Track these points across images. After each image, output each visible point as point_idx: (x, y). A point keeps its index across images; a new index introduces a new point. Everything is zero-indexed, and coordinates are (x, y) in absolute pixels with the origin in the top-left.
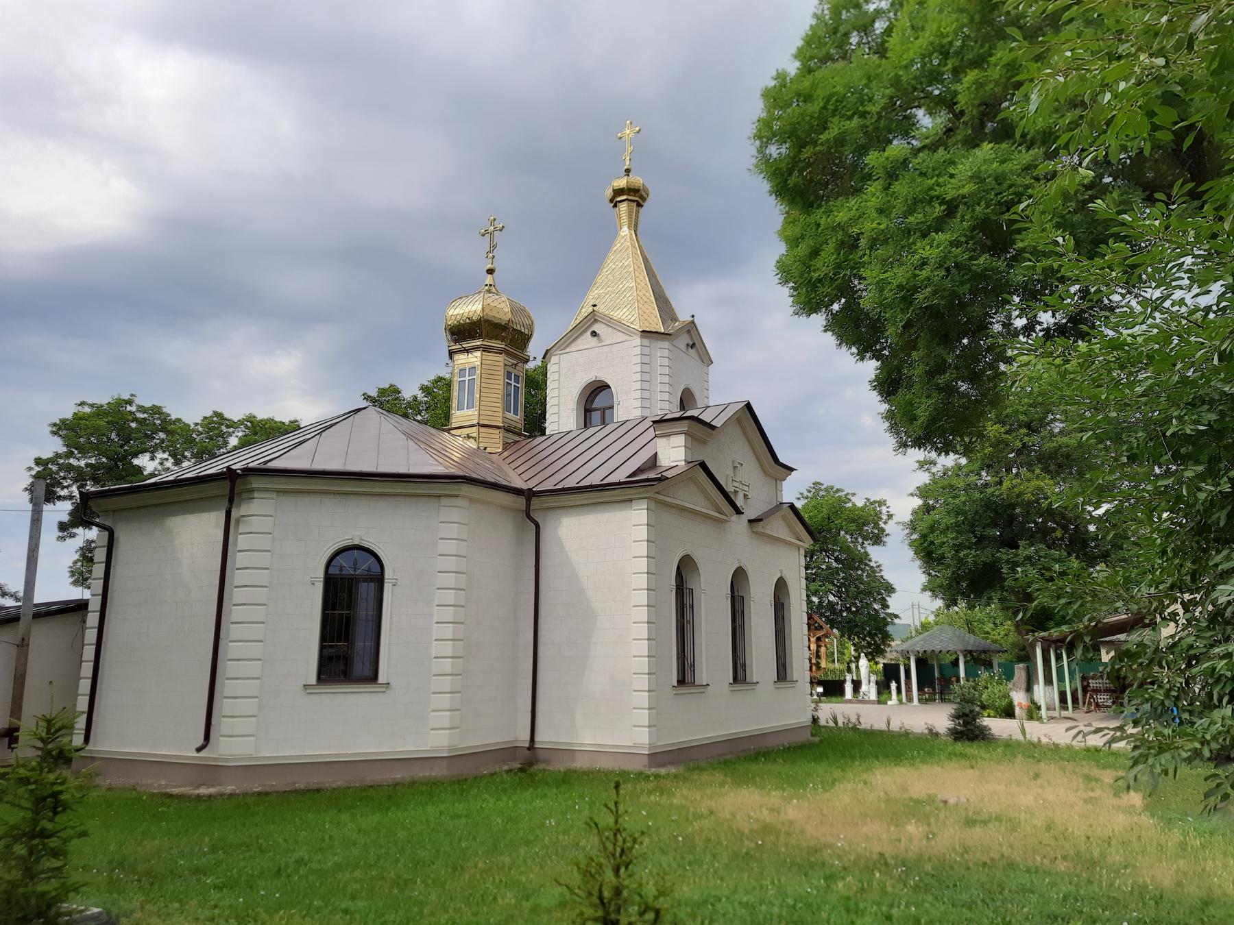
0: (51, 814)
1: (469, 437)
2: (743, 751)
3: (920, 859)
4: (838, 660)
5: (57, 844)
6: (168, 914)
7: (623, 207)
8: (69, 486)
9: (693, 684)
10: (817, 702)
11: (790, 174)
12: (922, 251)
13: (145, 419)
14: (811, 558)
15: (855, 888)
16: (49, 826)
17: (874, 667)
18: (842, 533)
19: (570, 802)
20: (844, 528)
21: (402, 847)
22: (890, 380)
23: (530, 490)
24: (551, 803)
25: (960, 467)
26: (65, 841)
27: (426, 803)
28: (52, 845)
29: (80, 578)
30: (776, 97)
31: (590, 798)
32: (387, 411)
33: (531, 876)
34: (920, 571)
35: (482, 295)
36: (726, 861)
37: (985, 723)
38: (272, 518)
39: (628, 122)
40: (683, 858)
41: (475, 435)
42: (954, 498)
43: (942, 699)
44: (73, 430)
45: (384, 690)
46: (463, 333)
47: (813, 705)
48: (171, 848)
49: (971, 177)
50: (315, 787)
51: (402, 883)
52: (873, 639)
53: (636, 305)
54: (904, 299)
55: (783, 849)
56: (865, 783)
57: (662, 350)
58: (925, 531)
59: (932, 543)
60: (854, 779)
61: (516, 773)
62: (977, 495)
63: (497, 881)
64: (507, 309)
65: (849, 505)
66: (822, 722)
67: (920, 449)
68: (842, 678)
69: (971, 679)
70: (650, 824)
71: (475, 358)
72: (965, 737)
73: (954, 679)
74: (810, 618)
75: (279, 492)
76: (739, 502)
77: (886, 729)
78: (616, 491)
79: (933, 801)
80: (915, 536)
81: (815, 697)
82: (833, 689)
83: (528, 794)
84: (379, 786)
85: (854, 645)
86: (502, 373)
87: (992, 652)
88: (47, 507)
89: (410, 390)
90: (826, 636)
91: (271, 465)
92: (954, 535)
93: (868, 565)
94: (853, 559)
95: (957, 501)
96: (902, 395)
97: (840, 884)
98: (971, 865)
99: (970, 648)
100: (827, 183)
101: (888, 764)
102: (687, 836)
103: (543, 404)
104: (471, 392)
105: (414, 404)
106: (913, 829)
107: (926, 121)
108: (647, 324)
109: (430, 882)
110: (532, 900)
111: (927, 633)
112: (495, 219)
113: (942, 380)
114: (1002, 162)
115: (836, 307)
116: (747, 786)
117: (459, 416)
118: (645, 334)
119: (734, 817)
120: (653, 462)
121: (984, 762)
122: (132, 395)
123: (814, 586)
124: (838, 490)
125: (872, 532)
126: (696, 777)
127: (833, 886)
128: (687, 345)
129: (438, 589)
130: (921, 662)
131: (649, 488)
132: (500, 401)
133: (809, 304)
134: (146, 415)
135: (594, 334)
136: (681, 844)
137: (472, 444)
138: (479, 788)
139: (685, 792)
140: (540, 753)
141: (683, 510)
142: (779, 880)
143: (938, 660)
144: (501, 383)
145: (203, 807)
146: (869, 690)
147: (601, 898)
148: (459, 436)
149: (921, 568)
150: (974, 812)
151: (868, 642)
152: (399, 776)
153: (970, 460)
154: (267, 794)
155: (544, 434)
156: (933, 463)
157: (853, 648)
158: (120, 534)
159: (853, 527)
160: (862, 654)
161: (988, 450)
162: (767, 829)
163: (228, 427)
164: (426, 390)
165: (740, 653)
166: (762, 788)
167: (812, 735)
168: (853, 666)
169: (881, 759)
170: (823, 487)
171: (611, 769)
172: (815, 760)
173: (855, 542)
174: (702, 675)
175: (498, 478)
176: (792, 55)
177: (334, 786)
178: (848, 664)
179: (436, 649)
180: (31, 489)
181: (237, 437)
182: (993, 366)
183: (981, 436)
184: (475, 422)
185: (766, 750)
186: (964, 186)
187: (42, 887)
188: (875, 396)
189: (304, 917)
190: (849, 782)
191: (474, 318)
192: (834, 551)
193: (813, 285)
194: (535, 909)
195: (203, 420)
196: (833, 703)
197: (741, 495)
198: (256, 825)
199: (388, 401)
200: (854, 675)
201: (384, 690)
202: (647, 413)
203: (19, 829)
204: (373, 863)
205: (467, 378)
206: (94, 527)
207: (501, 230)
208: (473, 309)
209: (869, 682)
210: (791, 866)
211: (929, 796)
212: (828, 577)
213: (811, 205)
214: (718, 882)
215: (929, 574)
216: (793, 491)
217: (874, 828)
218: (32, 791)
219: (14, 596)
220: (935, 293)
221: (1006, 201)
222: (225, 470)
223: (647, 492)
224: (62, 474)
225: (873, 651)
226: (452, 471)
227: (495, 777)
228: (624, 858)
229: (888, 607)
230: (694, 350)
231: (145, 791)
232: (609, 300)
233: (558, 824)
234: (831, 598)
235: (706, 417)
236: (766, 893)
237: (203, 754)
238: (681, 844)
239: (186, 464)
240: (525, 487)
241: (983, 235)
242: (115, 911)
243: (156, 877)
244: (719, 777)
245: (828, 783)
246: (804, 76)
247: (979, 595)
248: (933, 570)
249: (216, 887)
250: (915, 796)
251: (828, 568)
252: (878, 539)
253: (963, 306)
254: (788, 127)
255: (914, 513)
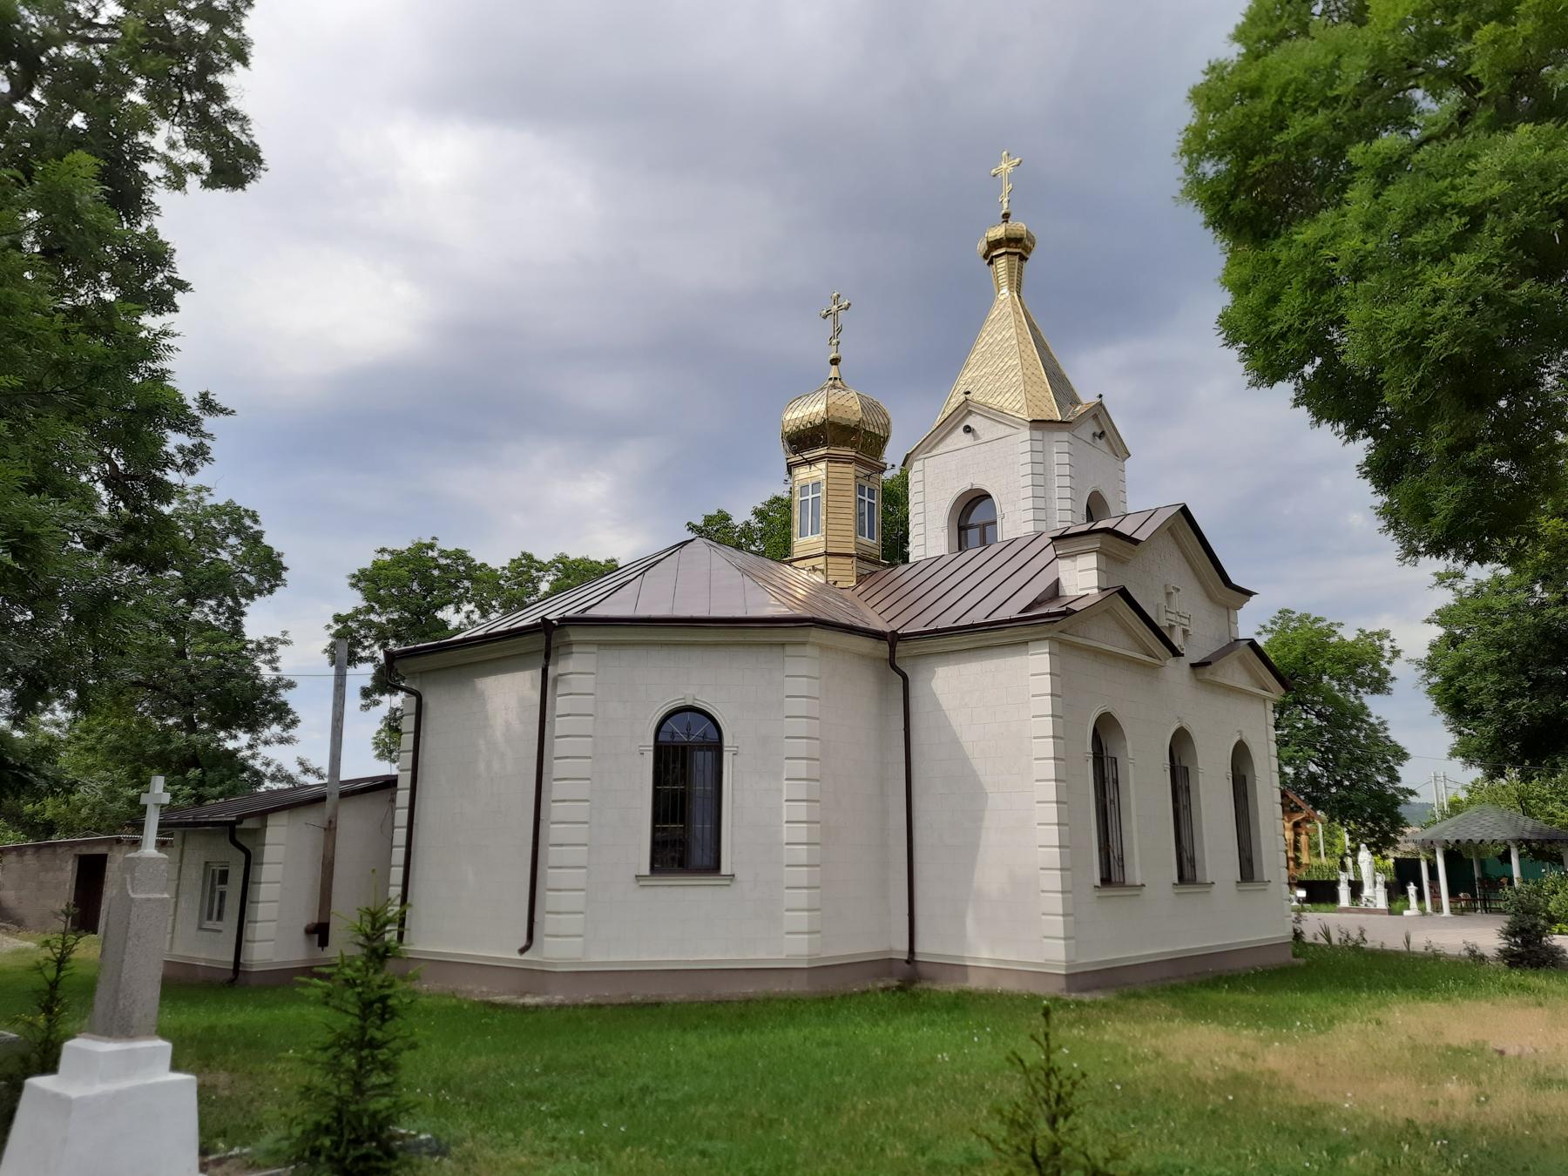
0: (378, 1022)
1: (814, 569)
2: (1196, 974)
3: (1468, 1129)
4: (1325, 854)
5: (385, 1057)
6: (502, 1146)
7: (1002, 263)
8: (371, 646)
9: (1122, 884)
10: (1299, 911)
11: (1233, 196)
12: (1437, 280)
13: (448, 565)
14: (1281, 714)
15: (1373, 1164)
16: (379, 1035)
17: (1380, 863)
18: (1325, 678)
19: (967, 1032)
20: (1328, 671)
21: (763, 1079)
22: (1387, 463)
23: (894, 632)
24: (942, 1033)
25: (1500, 581)
26: (397, 1052)
27: (787, 1026)
28: (381, 1057)
29: (386, 750)
30: (1208, 97)
31: (993, 1029)
32: (718, 543)
33: (926, 1124)
34: (1446, 729)
35: (825, 392)
36: (1186, 1120)
37: (1555, 943)
38: (593, 676)
39: (1005, 153)
40: (1124, 1112)
41: (822, 567)
42: (1494, 624)
43: (1486, 909)
44: (375, 582)
45: (728, 882)
46: (803, 441)
47: (1294, 915)
48: (499, 1067)
49: (1502, 174)
50: (654, 1000)
51: (766, 1123)
52: (1377, 824)
53: (1022, 388)
54: (1408, 350)
55: (1265, 1109)
56: (1379, 1023)
57: (1059, 448)
58: (1451, 673)
59: (1462, 689)
60: (1361, 1018)
61: (894, 992)
62: (1529, 619)
63: (883, 1127)
64: (857, 407)
65: (1334, 640)
66: (1308, 938)
67: (1438, 557)
68: (1333, 878)
69: (1531, 881)
70: (1075, 1065)
71: (819, 471)
72: (1525, 962)
73: (1504, 880)
74: (1284, 795)
75: (600, 644)
76: (1177, 640)
77: (1405, 949)
78: (1006, 631)
79: (1482, 1049)
80: (1435, 680)
81: (1295, 903)
82: (1321, 892)
83: (912, 1019)
84: (728, 1002)
85: (1349, 832)
86: (853, 487)
87: (1562, 841)
88: (350, 671)
89: (741, 515)
90: (1307, 820)
91: (591, 613)
92: (1496, 677)
93: (1366, 722)
94: (1342, 714)
95: (1498, 629)
96: (1409, 483)
97: (1352, 1160)
98: (1548, 1142)
99: (1527, 836)
100: (1287, 205)
101: (1410, 997)
102: (1127, 1084)
103: (905, 523)
104: (815, 514)
105: (747, 530)
106: (1455, 1089)
107: (1428, 105)
108: (1037, 411)
109: (801, 1123)
110: (929, 1155)
111: (1459, 816)
112: (839, 296)
113: (1473, 457)
114: (1548, 149)
115: (1308, 370)
116: (1206, 1021)
117: (804, 543)
118: (1034, 424)
119: (1191, 1062)
120: (1054, 591)
121: (1557, 998)
122: (434, 538)
123: (1289, 751)
124: (1317, 620)
125: (1370, 676)
126: (1132, 1007)
127: (1341, 1161)
128: (1094, 434)
129: (787, 758)
130: (1453, 856)
131: (1049, 626)
132: (853, 523)
133: (1268, 370)
134: (449, 561)
135: (968, 429)
136: (1120, 1095)
137: (819, 578)
138: (849, 1008)
139: (1119, 1026)
140: (921, 968)
141: (1097, 653)
142: (1263, 1149)
143: (1479, 853)
144: (852, 500)
145: (530, 1019)
146: (1375, 894)
147: (1034, 1156)
148: (803, 569)
149: (1446, 724)
150: (1547, 1068)
151: (1370, 829)
152: (751, 991)
153: (1518, 571)
154: (600, 1006)
155: (905, 560)
156: (1460, 576)
157: (1347, 837)
158: (428, 699)
159: (1340, 669)
160: (1363, 846)
161: (1544, 555)
162: (1238, 1080)
163: (538, 570)
164: (759, 513)
165: (1185, 843)
166: (1228, 1025)
167: (1295, 956)
168: (1349, 861)
169: (1399, 990)
170: (1294, 616)
171: (1016, 992)
172: (1302, 990)
173: (1346, 689)
174: (1135, 871)
175: (853, 619)
176: (1229, 36)
177: (675, 1000)
178: (1342, 858)
179: (787, 832)
180: (332, 651)
181: (548, 581)
182: (1546, 436)
183: (1534, 536)
184: (822, 551)
185: (1230, 974)
186: (1491, 186)
187: (373, 1106)
188: (1367, 486)
189: (655, 1157)
190: (1354, 1020)
191: (816, 422)
192: (1314, 703)
193: (1271, 343)
194: (934, 1166)
195: (510, 564)
196: (1321, 912)
197: (1178, 631)
198: (591, 1043)
199: (716, 530)
200: (1351, 873)
201: (728, 882)
202: (1042, 527)
203: (346, 1038)
204: (729, 1096)
205: (810, 497)
206: (399, 693)
207: (846, 309)
208: (815, 410)
209: (1375, 883)
210: (1278, 1130)
211: (1476, 1043)
212: (1309, 738)
213: (1266, 235)
214: (1178, 1147)
215: (1460, 733)
216: (1251, 623)
217: (1396, 1085)
218: (359, 994)
219: (317, 773)
220: (1455, 337)
221: (1557, 204)
222: (539, 621)
223: (1049, 630)
224: (362, 632)
225: (1378, 842)
226: (798, 612)
227: (868, 996)
228: (1062, 1106)
229: (1398, 779)
230: (1103, 441)
231: (465, 999)
232: (986, 384)
233: (953, 1060)
234: (1313, 768)
235: (1126, 528)
236: (1246, 1165)
237: (527, 956)
238: (1120, 1095)
239: (493, 616)
240: (888, 629)
241: (1524, 253)
242: (444, 1139)
243: (484, 1101)
244: (1165, 1007)
245: (1323, 1021)
246: (1250, 64)
247: (1536, 763)
248: (1466, 726)
249: (552, 1115)
250: (1455, 1043)
251: (1306, 727)
252: (1379, 685)
253: (1497, 353)
254: (1229, 134)
255: (1433, 647)
